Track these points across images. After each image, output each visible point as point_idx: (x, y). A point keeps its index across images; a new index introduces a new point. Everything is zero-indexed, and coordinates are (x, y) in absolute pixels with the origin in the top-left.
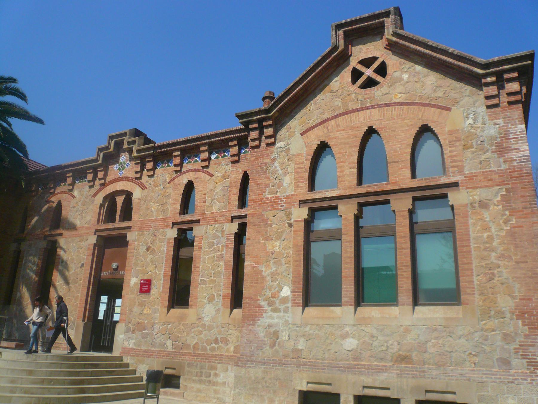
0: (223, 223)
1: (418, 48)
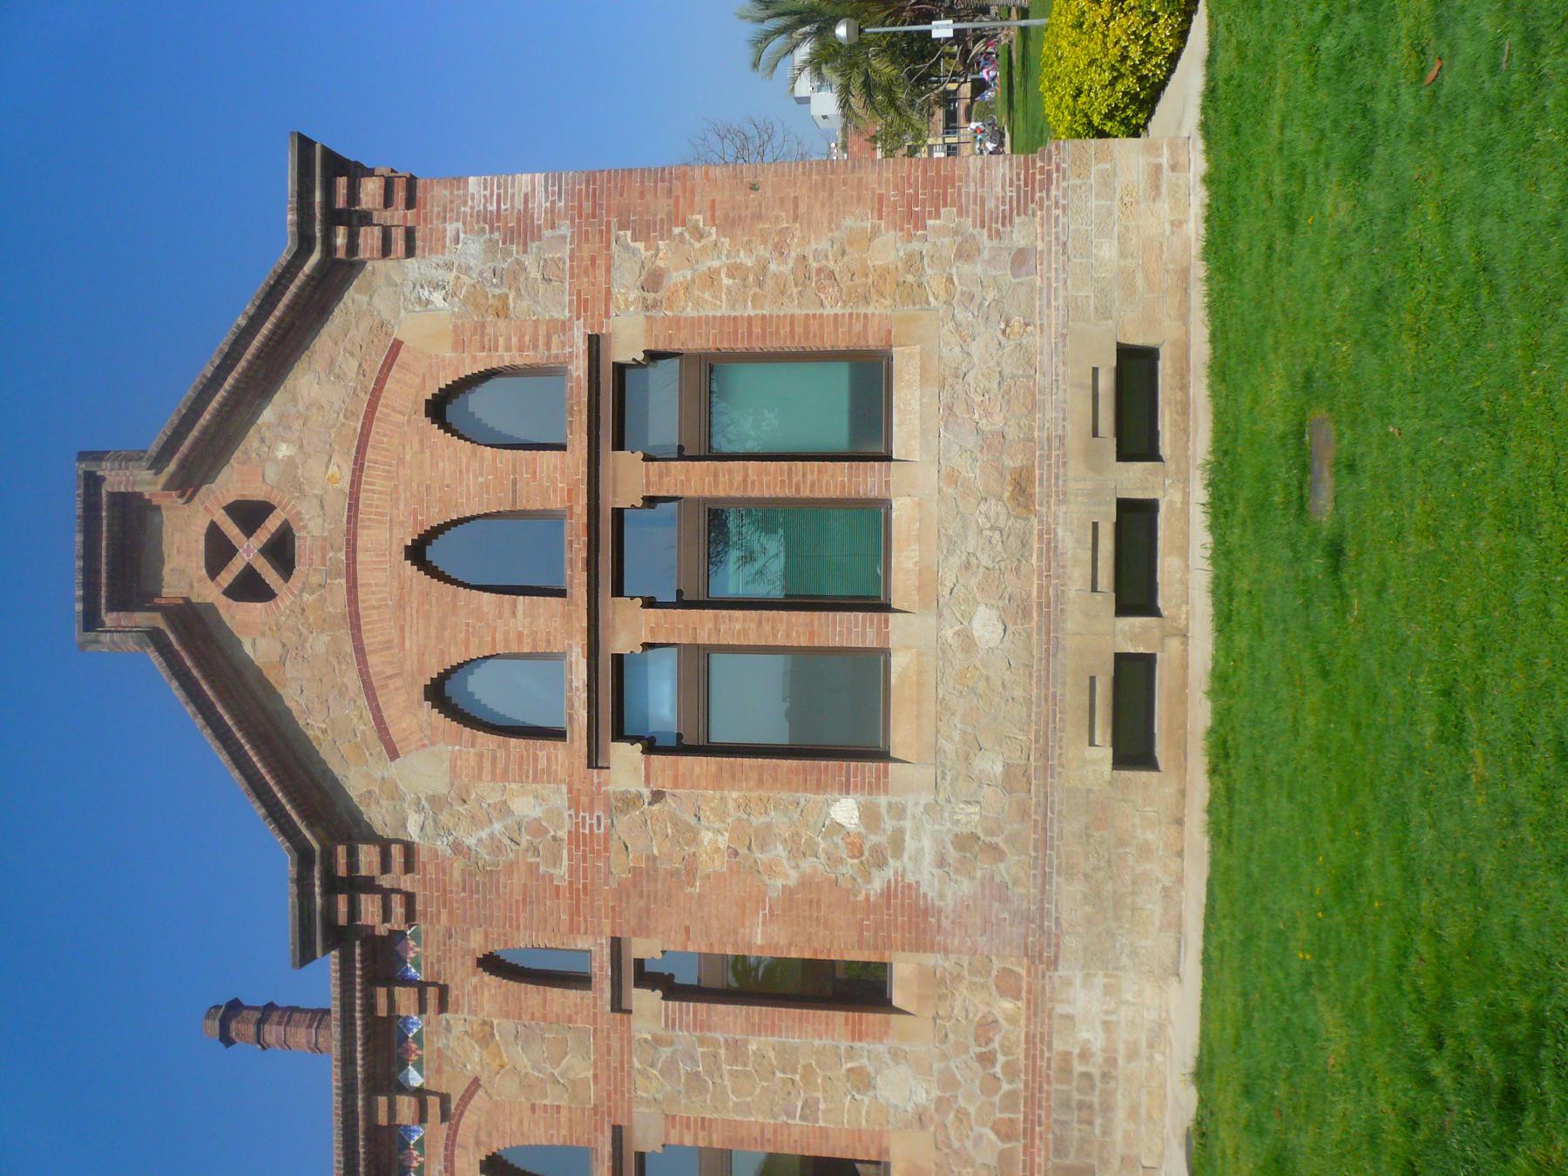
0: (629, 1042)
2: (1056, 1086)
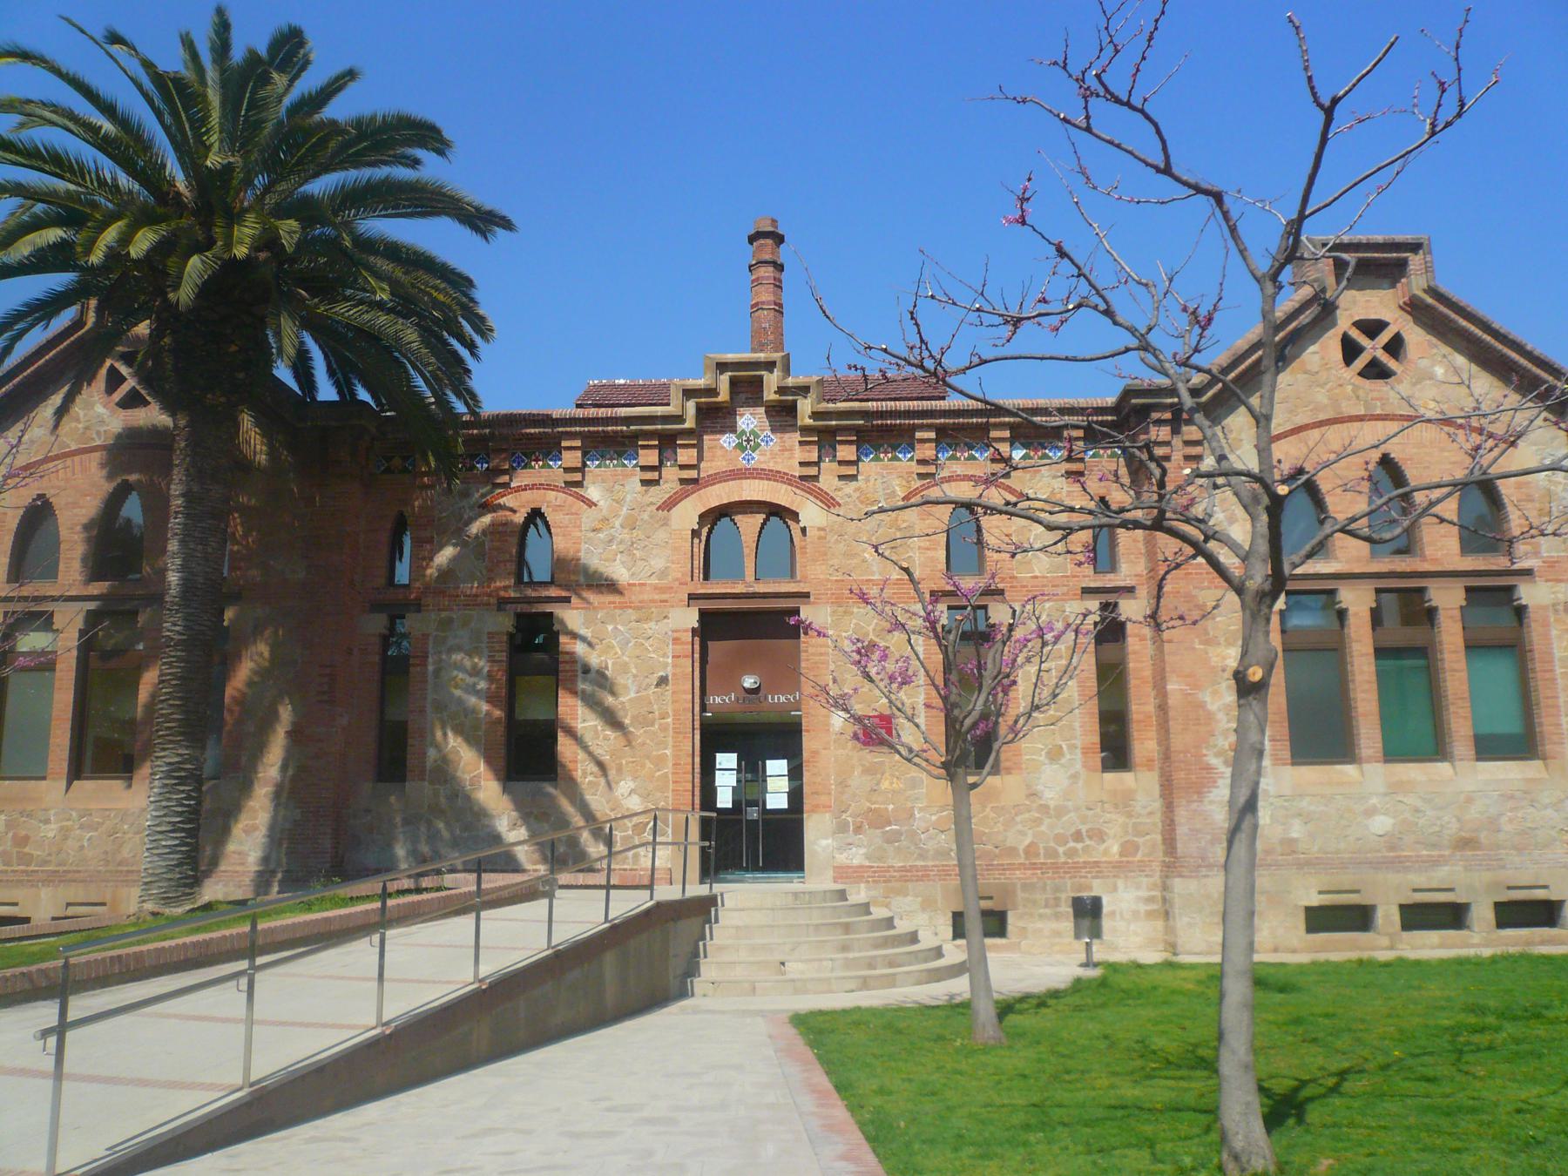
1: (1472, 328)
2: (1069, 882)
